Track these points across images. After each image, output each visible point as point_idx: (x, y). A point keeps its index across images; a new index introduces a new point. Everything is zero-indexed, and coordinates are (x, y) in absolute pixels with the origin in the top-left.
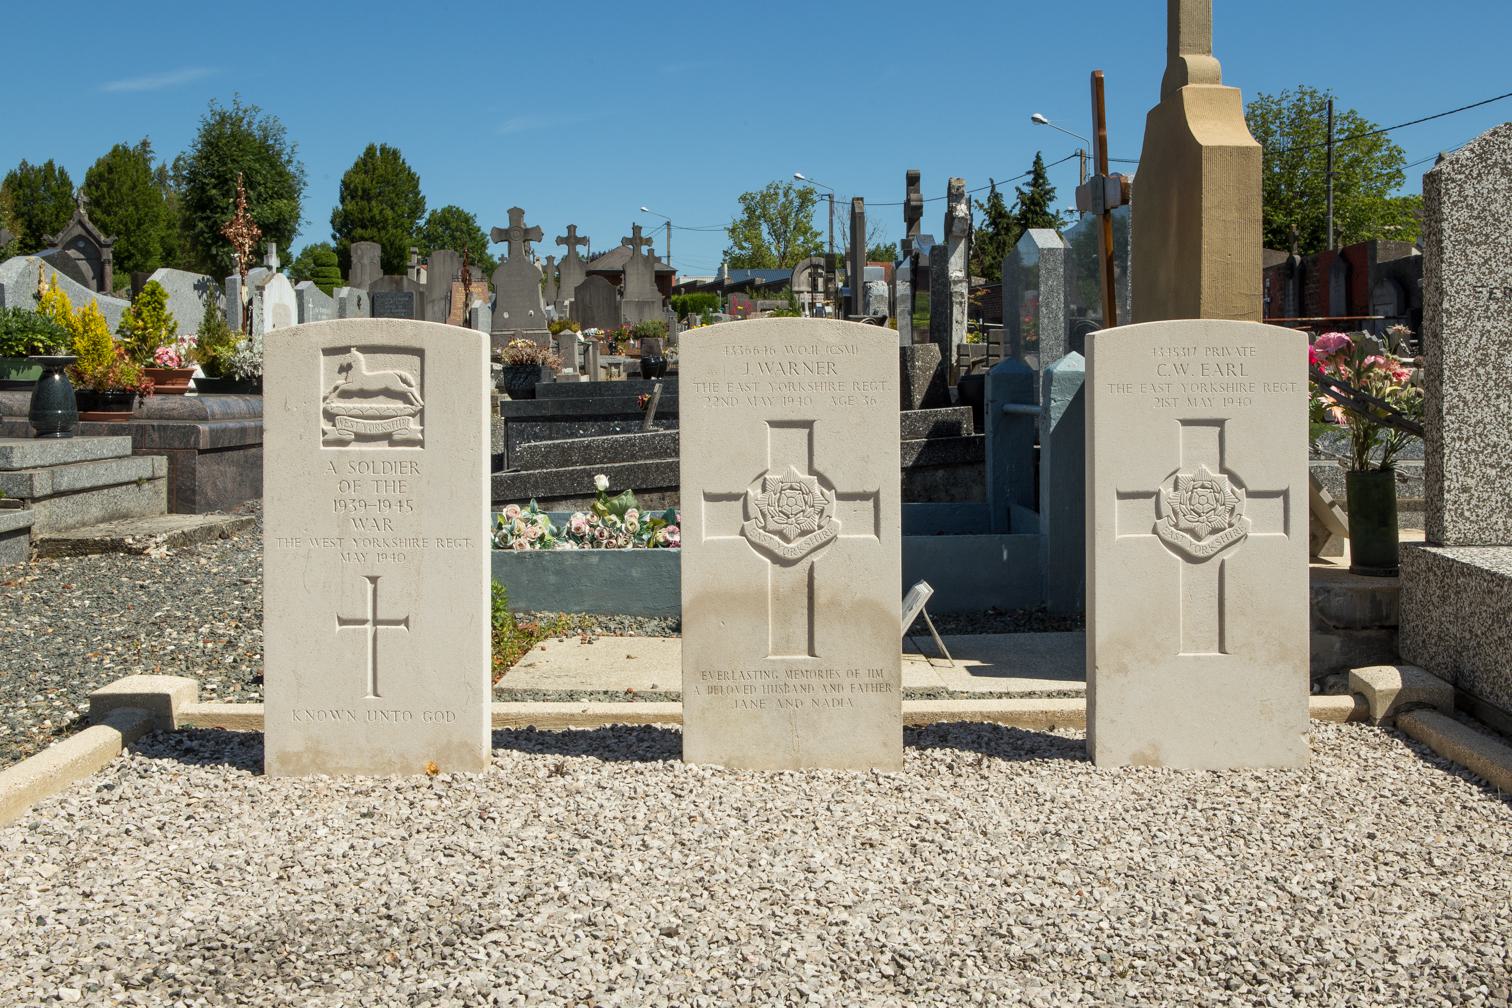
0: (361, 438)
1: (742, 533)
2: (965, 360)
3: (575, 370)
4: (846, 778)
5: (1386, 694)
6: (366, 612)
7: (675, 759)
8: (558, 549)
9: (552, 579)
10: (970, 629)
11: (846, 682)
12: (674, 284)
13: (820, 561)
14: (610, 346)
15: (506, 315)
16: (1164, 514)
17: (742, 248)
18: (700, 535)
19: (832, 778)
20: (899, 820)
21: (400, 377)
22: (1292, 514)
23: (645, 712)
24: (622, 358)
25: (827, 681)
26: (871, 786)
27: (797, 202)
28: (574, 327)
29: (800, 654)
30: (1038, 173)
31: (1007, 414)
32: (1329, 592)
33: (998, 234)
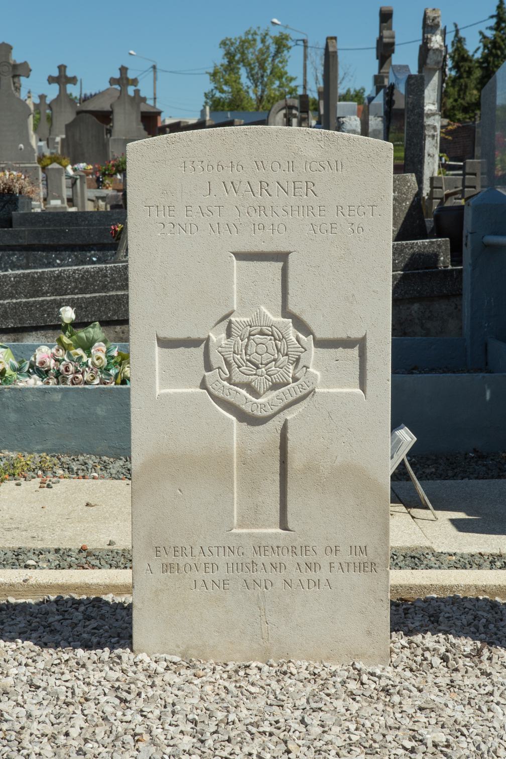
1: (203, 385)
2: (438, 193)
3: (63, 202)
4: (324, 675)
7: (123, 647)
8: (21, 385)
9: (13, 417)
10: (450, 473)
11: (324, 561)
12: (159, 125)
13: (294, 419)
14: (98, 179)
17: (222, 91)
18: (152, 387)
19: (305, 674)
20: (389, 738)
23: (95, 581)
24: (104, 192)
25: (302, 559)
26: (353, 686)
27: (273, 49)
28: (64, 162)
29: (270, 526)
31: (487, 246)
33: (460, 77)
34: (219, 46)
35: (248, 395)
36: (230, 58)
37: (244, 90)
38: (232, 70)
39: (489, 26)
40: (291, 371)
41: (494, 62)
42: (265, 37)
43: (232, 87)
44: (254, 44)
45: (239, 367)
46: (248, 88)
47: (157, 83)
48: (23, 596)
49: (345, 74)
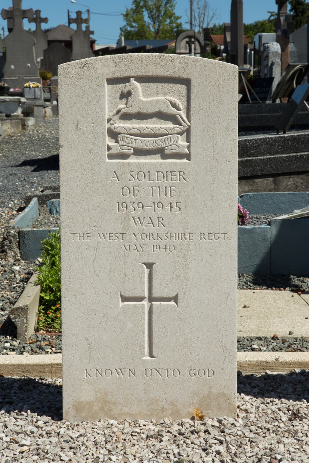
0: (139, 152)
6: (144, 291)
15: (13, 67)
17: (132, 26)
21: (171, 102)
33: (297, 16)
36: (136, 5)
37: (146, 25)
38: (139, 12)
46: (149, 24)
48: (275, 370)
49: (214, 14)
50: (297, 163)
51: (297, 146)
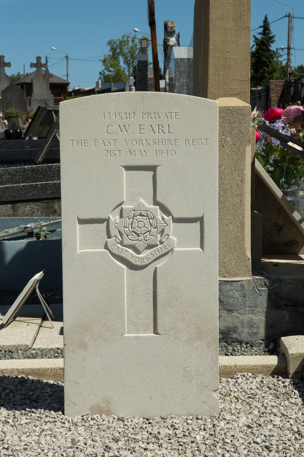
1: (106, 247)
5: (296, 356)
16: (112, 235)
17: (109, 71)
22: (206, 234)
30: (266, 27)
32: (281, 281)
34: (106, 44)
35: (133, 253)
37: (122, 70)
39: (259, 32)
40: (159, 237)
41: (262, 53)
42: (134, 39)
43: (114, 68)
44: (128, 43)
45: (127, 236)
46: (125, 69)
47: (69, 66)
50: (32, 192)
51: (36, 176)
